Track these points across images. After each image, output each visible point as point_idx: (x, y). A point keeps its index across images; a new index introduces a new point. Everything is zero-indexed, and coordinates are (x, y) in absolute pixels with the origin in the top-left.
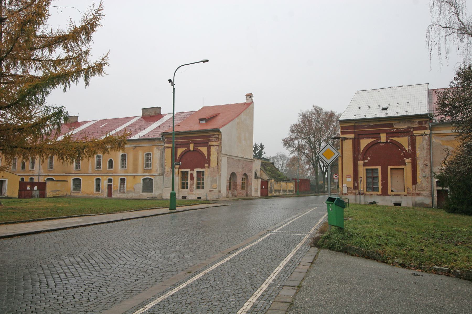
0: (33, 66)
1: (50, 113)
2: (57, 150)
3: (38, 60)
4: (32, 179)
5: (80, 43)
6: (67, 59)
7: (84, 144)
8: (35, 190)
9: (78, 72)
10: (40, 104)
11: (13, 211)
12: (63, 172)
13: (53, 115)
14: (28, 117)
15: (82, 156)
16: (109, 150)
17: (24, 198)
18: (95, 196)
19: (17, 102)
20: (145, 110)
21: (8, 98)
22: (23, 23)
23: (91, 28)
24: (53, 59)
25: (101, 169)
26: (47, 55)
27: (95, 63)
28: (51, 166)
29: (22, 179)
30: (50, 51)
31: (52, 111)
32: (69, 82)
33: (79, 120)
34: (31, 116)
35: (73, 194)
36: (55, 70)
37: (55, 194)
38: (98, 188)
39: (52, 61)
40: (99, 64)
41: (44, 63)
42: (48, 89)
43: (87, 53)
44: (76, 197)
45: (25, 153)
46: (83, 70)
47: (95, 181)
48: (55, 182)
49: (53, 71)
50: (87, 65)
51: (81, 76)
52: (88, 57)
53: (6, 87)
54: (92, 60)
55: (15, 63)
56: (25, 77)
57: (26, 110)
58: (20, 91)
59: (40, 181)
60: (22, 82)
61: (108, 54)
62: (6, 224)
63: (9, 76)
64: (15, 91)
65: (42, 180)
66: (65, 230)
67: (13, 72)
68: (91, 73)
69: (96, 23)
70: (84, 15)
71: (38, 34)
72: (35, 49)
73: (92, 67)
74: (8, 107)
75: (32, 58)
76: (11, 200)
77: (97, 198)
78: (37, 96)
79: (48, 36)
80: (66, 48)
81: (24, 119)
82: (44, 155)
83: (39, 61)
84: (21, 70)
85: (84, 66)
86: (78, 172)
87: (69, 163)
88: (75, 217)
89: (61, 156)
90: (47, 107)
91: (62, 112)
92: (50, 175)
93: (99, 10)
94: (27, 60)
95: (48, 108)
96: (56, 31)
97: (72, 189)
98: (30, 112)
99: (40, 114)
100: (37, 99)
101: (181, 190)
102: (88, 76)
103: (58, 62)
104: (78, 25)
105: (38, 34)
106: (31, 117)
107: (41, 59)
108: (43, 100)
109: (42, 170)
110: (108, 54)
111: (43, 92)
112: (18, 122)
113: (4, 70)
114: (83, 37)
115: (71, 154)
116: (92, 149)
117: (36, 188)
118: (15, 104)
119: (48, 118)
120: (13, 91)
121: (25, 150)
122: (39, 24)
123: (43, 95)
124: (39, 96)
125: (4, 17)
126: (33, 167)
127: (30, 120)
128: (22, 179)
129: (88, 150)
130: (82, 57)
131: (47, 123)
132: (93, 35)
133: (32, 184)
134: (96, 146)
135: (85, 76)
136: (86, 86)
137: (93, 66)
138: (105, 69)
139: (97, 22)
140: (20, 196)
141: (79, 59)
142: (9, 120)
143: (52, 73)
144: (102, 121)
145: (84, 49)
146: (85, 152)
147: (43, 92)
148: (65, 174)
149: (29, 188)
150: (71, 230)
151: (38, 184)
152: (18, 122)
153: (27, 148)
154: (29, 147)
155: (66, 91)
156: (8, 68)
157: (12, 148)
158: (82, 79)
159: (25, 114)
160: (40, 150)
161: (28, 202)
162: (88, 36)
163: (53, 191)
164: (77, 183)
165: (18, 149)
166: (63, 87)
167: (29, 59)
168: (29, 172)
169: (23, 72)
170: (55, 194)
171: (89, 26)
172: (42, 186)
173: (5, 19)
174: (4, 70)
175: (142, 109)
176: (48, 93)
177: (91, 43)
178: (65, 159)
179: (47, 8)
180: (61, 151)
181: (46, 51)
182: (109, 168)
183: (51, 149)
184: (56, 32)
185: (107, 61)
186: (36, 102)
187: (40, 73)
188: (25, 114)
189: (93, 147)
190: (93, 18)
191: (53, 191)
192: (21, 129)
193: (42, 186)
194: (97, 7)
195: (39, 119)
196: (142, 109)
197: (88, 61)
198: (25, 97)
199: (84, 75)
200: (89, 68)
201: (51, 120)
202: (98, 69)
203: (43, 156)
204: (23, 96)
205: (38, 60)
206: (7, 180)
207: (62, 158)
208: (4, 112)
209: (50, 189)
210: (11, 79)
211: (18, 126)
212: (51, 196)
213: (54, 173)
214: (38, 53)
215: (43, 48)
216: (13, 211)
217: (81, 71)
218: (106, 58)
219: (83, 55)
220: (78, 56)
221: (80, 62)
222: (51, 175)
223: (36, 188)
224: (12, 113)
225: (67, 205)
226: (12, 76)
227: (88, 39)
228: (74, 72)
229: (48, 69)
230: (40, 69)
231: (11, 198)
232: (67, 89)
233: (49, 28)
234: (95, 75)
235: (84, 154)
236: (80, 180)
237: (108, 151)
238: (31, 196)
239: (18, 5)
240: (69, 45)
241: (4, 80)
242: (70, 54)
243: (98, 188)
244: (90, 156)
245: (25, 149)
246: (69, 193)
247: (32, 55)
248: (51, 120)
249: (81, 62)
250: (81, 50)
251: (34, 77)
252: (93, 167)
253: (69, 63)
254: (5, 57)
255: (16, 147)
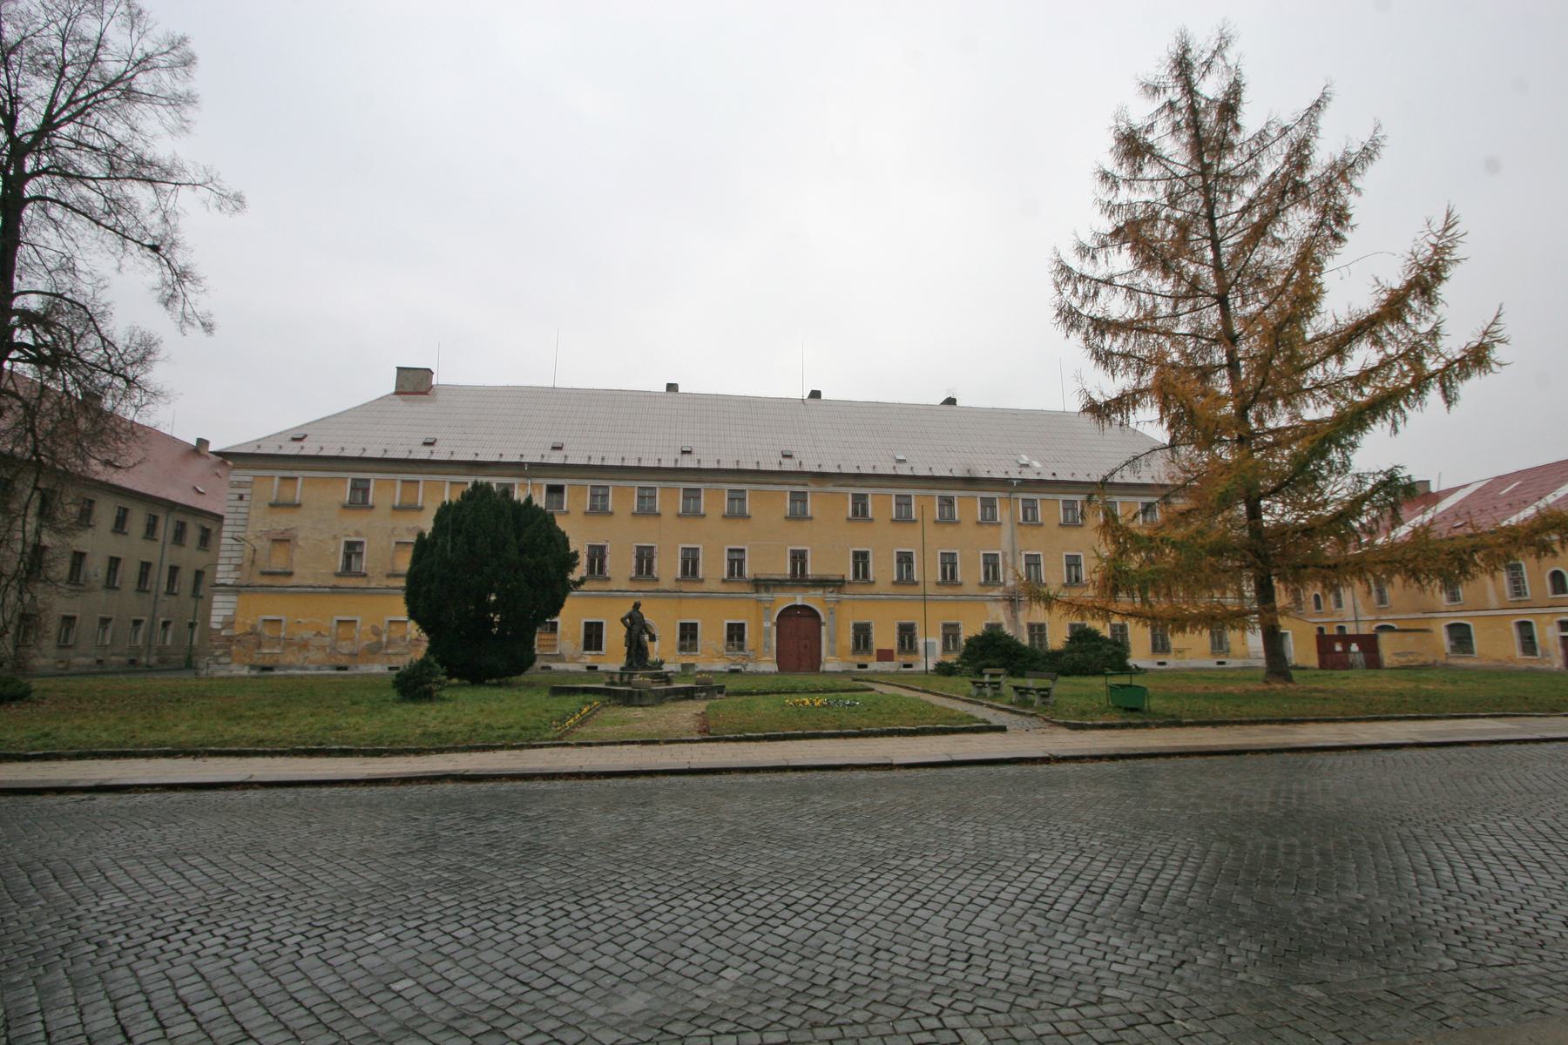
0: (1310, 401)
1: (1368, 487)
2: (1400, 562)
3: (1318, 386)
4: (1341, 628)
5: (1410, 319)
6: (1386, 363)
7: (1471, 541)
8: (1355, 653)
9: (1420, 383)
10: (1339, 473)
11: (1322, 695)
12: (1416, 611)
13: (1375, 489)
14: (1319, 504)
15: (1472, 569)
16: (1557, 547)
17: (1333, 668)
18: (1523, 666)
19: (1291, 480)
20: (405, 372)
21: (1271, 475)
22: (1278, 329)
23: (1432, 276)
24: (1351, 374)
25: (1528, 597)
26: (1337, 371)
27: (1464, 350)
28: (1382, 600)
29: (1321, 630)
30: (1341, 361)
31: (1371, 481)
32: (1402, 411)
33: (1434, 489)
34: (1326, 501)
35: (1452, 661)
36: (1361, 394)
37: (1403, 659)
38: (1528, 644)
39: (1350, 379)
40: (1477, 347)
41: (1332, 388)
42: (1353, 438)
43: (1434, 334)
44: (1466, 669)
45: (1324, 578)
46: (1433, 375)
47: (1515, 631)
48: (1397, 635)
49: (1357, 398)
50: (1442, 360)
51: (1431, 389)
52: (1440, 343)
53: (1263, 456)
54: (1454, 344)
55: (1273, 406)
56: (1297, 427)
57: (1312, 491)
58: (1294, 456)
59: (1362, 632)
60: (1295, 439)
61: (1498, 316)
62: (1316, 721)
63: (1263, 434)
64: (1282, 458)
65: (1365, 629)
66: (1467, 748)
67: (1271, 424)
68: (1457, 376)
69: (1443, 260)
70: (1410, 256)
71: (1309, 336)
72: (1310, 366)
73: (1457, 361)
74: (1276, 491)
75: (1305, 387)
76: (1307, 673)
77: (1531, 671)
78: (1331, 457)
79: (1330, 332)
80: (1377, 342)
81: (1311, 509)
82: (1369, 575)
83: (1322, 388)
84: (1286, 416)
85: (1431, 365)
86: (1459, 608)
87: (1437, 590)
88: (1484, 717)
89: (1414, 574)
90: (1357, 475)
91: (1397, 479)
92: (1384, 617)
93: (1446, 230)
94: (1293, 394)
95: (1360, 479)
96: (1347, 316)
97: (1448, 650)
98: (1321, 493)
99: (1345, 492)
100: (1330, 463)
101: (1476, 655)
102: (1451, 382)
103: (1366, 376)
104: (1397, 283)
105: (1309, 336)
106: (1325, 503)
107: (1325, 383)
108: (1346, 466)
109: (1361, 610)
110: (1498, 316)
111: (1342, 446)
112: (1299, 517)
113: (1254, 426)
114: (1415, 304)
115: (1441, 569)
116: (1498, 551)
117: (1354, 647)
118: (1287, 484)
119: (1367, 497)
120: (1277, 461)
121: (1324, 571)
122: (1309, 317)
123: (1343, 453)
124: (1335, 455)
125: (1237, 332)
126: (1339, 604)
127: (1324, 508)
128: (1321, 630)
129: (1487, 555)
130: (1424, 347)
131: (1365, 508)
132: (1443, 290)
133: (1347, 640)
134: (1509, 542)
135: (1443, 386)
136: (1448, 407)
137: (1458, 357)
138: (1498, 353)
139: (1447, 257)
140: (1323, 665)
141: (1414, 355)
142: (1283, 515)
143: (1352, 401)
144: (1503, 480)
145: (1424, 328)
146: (1478, 561)
147: (1342, 446)
148: (1420, 615)
149: (1338, 648)
150: (1482, 749)
151: (1361, 639)
152: (1299, 517)
153: (1329, 567)
154: (1331, 562)
155: (1396, 431)
156: (1260, 420)
157: (1297, 568)
158: (1434, 395)
159: (1309, 499)
160: (1358, 568)
161: (1347, 678)
162: (1429, 295)
163: (1398, 655)
164: (1461, 636)
165: (1310, 570)
166: (1387, 425)
167: (1300, 391)
168: (1332, 614)
169: (1291, 419)
170: (1403, 659)
171: (1427, 274)
172: (1369, 644)
173: (1241, 333)
174: (1254, 426)
175: (399, 369)
176: (1353, 445)
177: (1439, 309)
178: (1425, 582)
179: (1318, 280)
180: (1411, 566)
181: (1332, 364)
182: (1555, 592)
183: (1383, 562)
184: (1345, 319)
185: (1500, 334)
186: (1331, 471)
187: (1328, 412)
188: (1309, 499)
189: (1501, 546)
190: (1435, 253)
191: (1398, 655)
192: (1308, 531)
193: (1369, 644)
194: (1438, 225)
195: (1342, 503)
196: (399, 369)
197: (1442, 350)
198: (1306, 464)
199: (1437, 385)
200: (1449, 365)
201: (1372, 502)
202: (1474, 361)
203: (1367, 580)
204: (1300, 464)
205: (1318, 386)
206: (1290, 632)
207: (1418, 580)
208: (1268, 502)
209: (1388, 648)
210: (1269, 439)
211: (1302, 525)
212: (1396, 664)
213: (1392, 613)
214: (1317, 373)
215: (1323, 359)
216: (1322, 695)
217: (1427, 378)
218: (1495, 328)
219: (1425, 342)
220: (1413, 349)
221: (1419, 359)
222: (1386, 619)
223: (1354, 647)
224: (1284, 502)
225: (1449, 687)
226: (1271, 432)
227: (1431, 303)
228: (1409, 386)
229: (1344, 398)
230: (1325, 402)
231: (1304, 668)
232: (1400, 427)
233: (1329, 314)
234: (1468, 375)
235: (1476, 565)
236: (1467, 627)
237: (1553, 551)
238: (1347, 666)
239: (1259, 301)
240: (1384, 334)
241: (1257, 444)
242: (1391, 350)
243: (1528, 644)
244: (1496, 569)
245: (1323, 567)
246: (1441, 659)
247: (1304, 382)
248: (1372, 502)
249: (1423, 358)
250: (1415, 333)
251: (1314, 422)
252: (1500, 595)
253: (1391, 370)
254: (1253, 401)
255: (1305, 567)
